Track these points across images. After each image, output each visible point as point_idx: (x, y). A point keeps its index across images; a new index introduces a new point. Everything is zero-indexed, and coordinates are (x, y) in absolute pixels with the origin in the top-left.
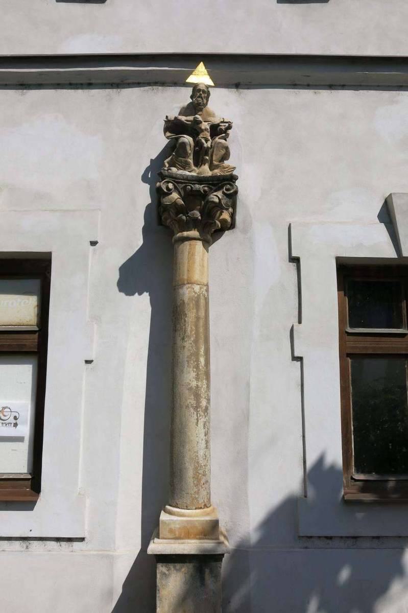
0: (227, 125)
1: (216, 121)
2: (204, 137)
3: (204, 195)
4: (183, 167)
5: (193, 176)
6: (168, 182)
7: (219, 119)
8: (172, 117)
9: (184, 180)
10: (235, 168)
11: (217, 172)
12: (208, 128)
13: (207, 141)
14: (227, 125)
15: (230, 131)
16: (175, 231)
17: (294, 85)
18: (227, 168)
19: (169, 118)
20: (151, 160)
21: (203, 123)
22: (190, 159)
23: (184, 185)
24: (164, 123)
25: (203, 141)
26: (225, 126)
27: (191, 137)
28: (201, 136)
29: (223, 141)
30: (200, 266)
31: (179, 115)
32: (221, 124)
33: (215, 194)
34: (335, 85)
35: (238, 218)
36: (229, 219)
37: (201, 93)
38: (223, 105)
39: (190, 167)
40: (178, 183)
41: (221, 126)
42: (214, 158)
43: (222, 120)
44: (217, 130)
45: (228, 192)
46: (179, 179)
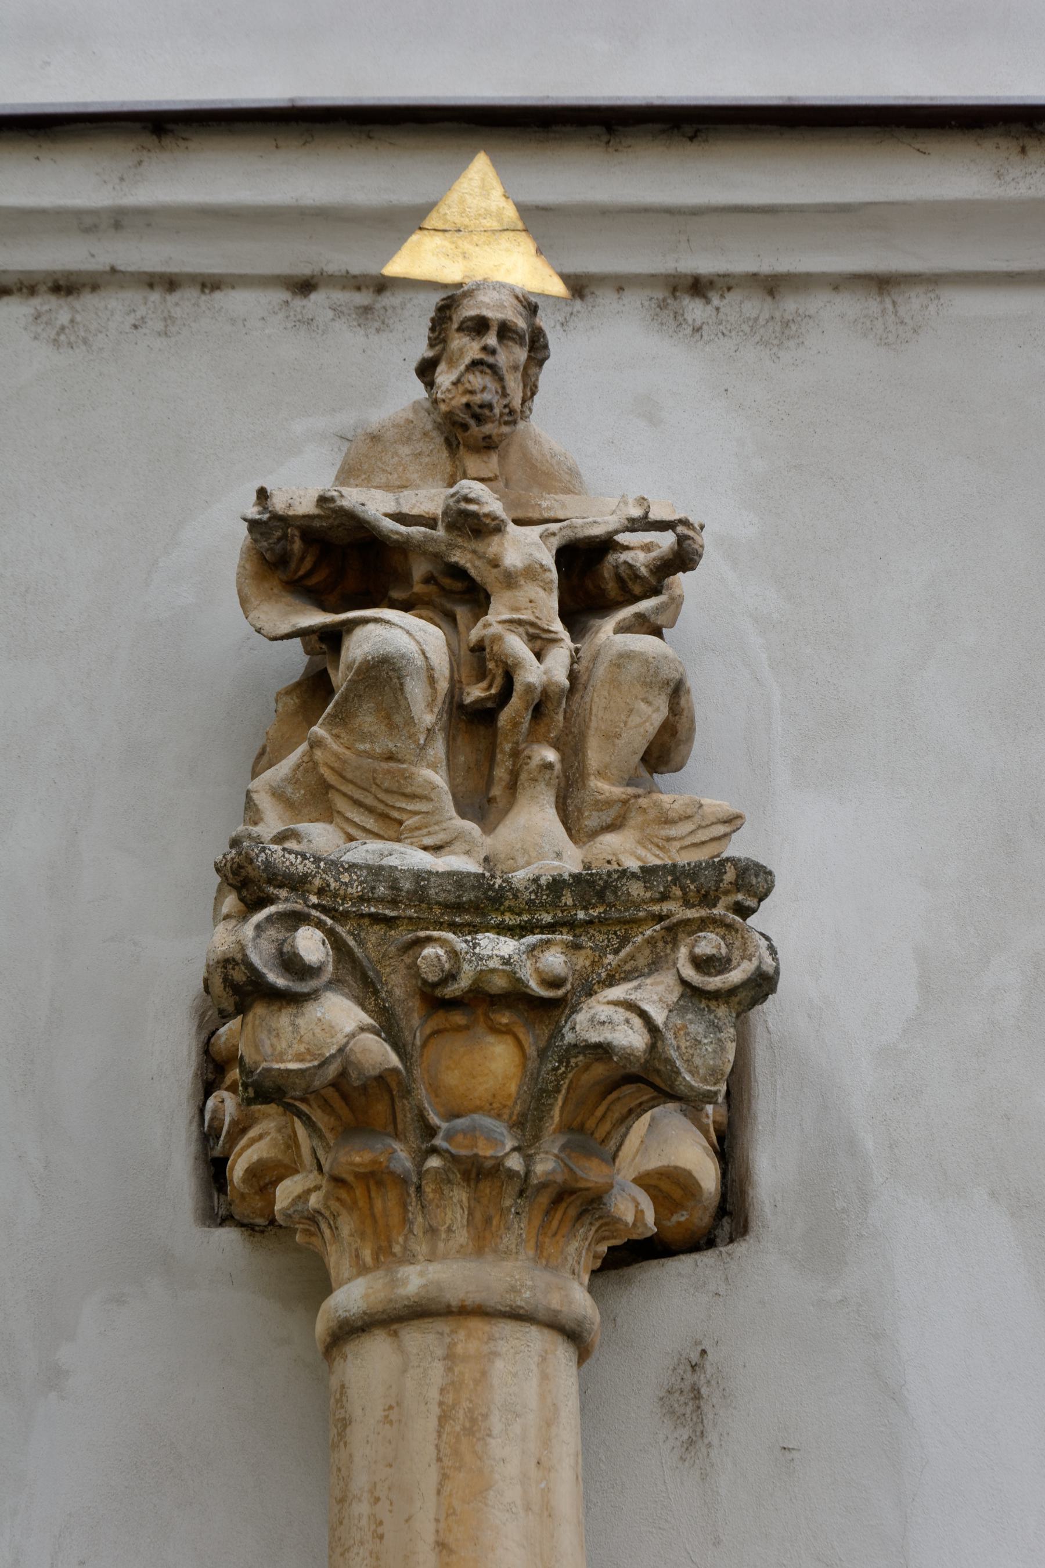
0: (666, 540)
1: (596, 515)
2: (520, 622)
4: (384, 817)
5: (458, 879)
6: (295, 920)
7: (613, 502)
10: (738, 817)
11: (624, 849)
12: (548, 559)
13: (540, 643)
14: (666, 540)
15: (683, 581)
16: (338, 1262)
19: (279, 504)
21: (511, 527)
22: (433, 766)
24: (242, 531)
25: (517, 646)
26: (647, 548)
28: (498, 612)
29: (643, 643)
30: (528, 1508)
31: (348, 473)
32: (623, 538)
33: (618, 992)
35: (772, 1165)
36: (707, 1174)
37: (491, 340)
38: (623, 431)
41: (627, 548)
42: (595, 756)
43: (636, 512)
44: (589, 579)
45: (715, 982)
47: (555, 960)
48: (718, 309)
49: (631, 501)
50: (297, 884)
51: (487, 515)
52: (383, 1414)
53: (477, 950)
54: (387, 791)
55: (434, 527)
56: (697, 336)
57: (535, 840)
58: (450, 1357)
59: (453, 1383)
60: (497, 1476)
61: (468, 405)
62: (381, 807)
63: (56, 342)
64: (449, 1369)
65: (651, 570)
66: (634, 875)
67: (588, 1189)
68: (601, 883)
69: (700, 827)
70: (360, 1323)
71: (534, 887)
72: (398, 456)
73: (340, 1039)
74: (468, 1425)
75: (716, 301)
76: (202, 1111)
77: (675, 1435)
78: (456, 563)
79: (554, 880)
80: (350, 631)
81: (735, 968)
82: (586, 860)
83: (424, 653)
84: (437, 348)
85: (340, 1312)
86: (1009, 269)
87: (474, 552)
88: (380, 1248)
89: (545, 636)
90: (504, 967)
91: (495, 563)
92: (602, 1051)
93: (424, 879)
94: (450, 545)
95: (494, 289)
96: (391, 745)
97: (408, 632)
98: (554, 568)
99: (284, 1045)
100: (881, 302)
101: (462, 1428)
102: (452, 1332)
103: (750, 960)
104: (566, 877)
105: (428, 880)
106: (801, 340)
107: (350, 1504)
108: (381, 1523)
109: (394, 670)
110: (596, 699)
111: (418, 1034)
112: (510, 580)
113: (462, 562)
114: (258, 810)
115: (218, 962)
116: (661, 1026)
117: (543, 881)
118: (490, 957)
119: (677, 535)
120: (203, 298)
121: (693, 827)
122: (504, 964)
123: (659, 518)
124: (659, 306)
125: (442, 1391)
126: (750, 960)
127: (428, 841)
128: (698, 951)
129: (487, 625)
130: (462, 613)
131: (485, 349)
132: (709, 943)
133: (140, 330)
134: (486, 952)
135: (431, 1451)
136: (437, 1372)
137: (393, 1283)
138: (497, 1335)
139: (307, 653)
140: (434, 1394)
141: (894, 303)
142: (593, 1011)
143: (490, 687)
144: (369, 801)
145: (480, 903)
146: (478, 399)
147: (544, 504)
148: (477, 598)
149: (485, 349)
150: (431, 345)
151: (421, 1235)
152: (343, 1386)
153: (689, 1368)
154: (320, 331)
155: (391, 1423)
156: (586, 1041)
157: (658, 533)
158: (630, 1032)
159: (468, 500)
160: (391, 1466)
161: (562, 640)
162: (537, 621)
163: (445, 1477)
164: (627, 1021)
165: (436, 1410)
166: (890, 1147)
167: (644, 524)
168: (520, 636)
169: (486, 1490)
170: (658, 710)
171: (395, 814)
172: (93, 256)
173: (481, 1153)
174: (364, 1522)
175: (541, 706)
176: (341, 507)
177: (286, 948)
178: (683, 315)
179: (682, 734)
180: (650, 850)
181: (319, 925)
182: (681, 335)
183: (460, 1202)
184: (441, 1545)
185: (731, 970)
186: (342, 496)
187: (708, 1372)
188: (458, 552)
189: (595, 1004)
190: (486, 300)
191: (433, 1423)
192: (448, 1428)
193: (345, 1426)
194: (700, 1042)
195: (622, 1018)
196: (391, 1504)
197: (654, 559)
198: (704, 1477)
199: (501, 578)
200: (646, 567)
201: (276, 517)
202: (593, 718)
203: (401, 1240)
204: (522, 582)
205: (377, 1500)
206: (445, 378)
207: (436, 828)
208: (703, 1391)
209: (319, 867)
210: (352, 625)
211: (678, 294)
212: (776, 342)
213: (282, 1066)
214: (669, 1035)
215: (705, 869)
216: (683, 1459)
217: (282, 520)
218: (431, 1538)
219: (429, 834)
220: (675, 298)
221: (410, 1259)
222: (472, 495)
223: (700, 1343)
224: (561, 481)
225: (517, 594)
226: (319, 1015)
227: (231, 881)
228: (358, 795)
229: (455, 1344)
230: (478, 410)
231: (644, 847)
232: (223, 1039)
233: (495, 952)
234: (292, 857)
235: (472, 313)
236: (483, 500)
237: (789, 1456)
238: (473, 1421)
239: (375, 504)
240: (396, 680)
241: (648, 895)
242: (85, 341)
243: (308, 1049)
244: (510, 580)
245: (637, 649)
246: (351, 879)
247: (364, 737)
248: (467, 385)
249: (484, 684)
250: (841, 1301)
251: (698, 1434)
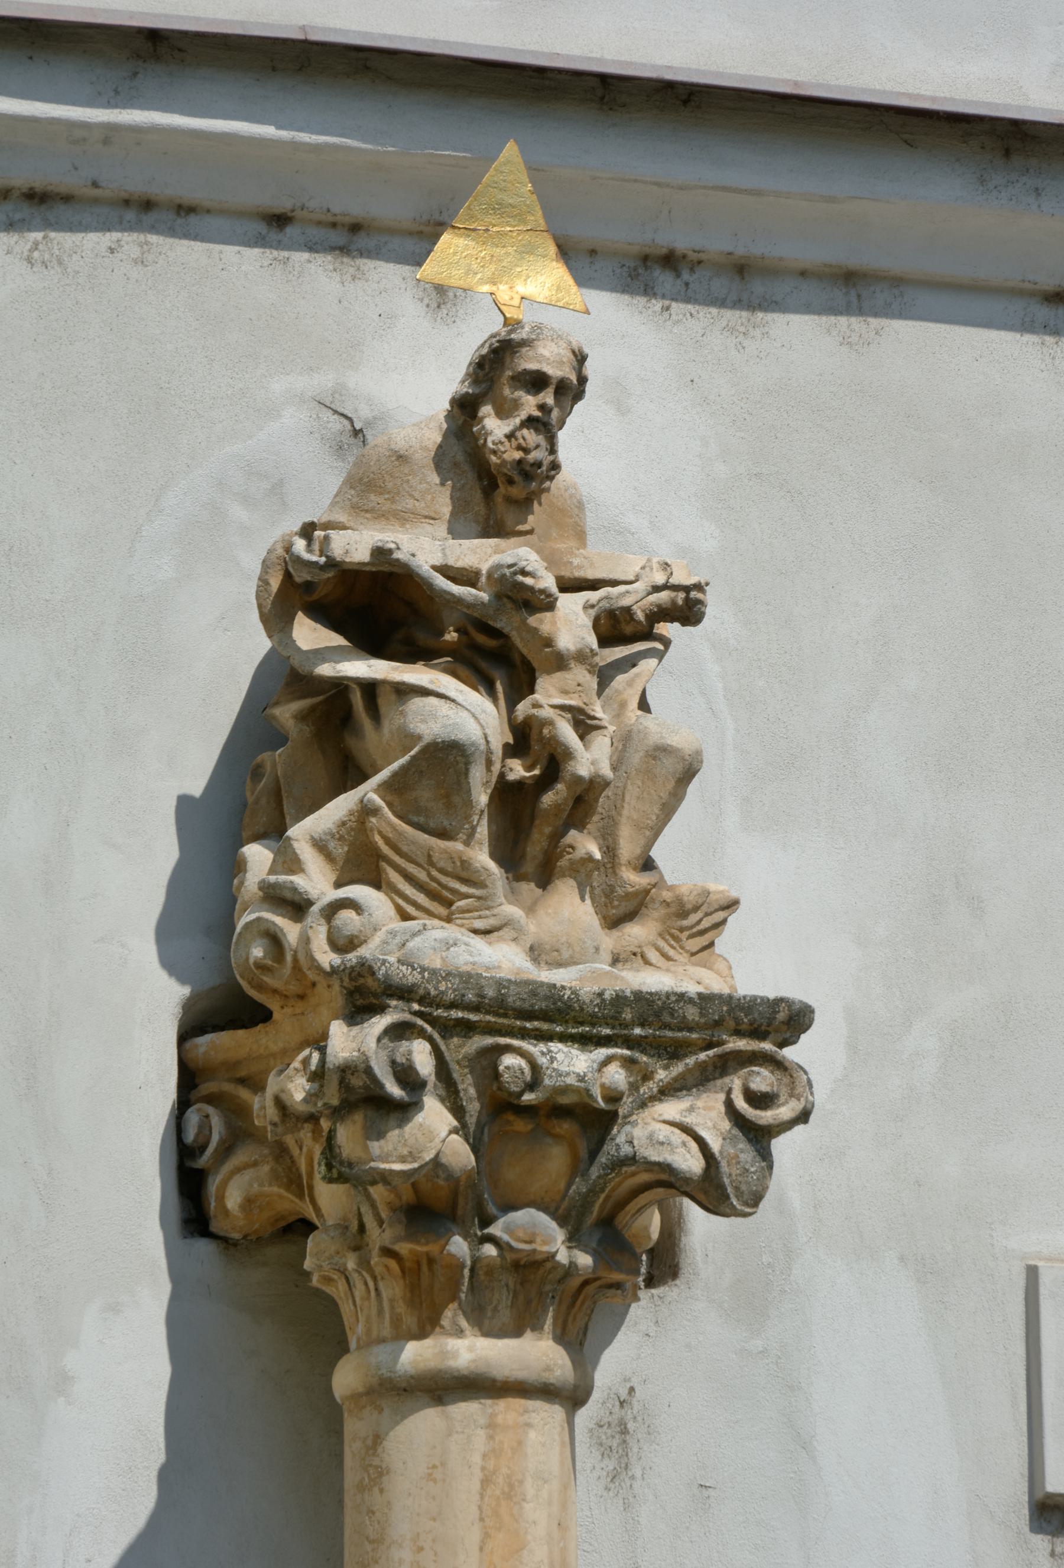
3: (592, 1120)
6: (399, 1032)
9: (476, 1008)
13: (585, 725)
16: (358, 1317)
18: (696, 909)
20: (184, 803)
23: (490, 1040)
25: (566, 732)
33: (672, 1109)
34: (897, 282)
37: (548, 397)
39: (484, 902)
40: (448, 1028)
43: (660, 579)
46: (453, 1005)
47: (617, 1076)
48: (687, 284)
49: (655, 566)
50: (405, 993)
52: (427, 1471)
53: (555, 1065)
54: (442, 871)
56: (666, 314)
58: (491, 1426)
59: (494, 1450)
60: (529, 1537)
61: (520, 462)
63: (29, 260)
64: (491, 1437)
65: (646, 615)
66: (691, 1001)
68: (659, 1003)
69: (707, 914)
70: (404, 1385)
71: (598, 1001)
72: (427, 483)
73: (436, 1144)
74: (506, 1489)
75: (686, 276)
77: (603, 1465)
79: (617, 995)
81: (783, 1105)
82: (615, 951)
83: (486, 738)
84: (484, 386)
85: (384, 1371)
89: (589, 722)
90: (579, 1084)
93: (504, 987)
95: (552, 340)
96: (446, 823)
97: (474, 716)
99: (391, 1147)
100: (847, 294)
101: (501, 1493)
103: (799, 1100)
104: (628, 993)
105: (508, 988)
106: (767, 329)
107: (389, 1547)
109: (462, 755)
111: (486, 1131)
112: (560, 662)
115: (339, 1067)
116: (717, 1154)
117: (607, 996)
118: (568, 1074)
120: (180, 221)
122: (579, 1081)
124: (630, 276)
125: (484, 1456)
126: (799, 1100)
127: (479, 924)
128: (753, 1086)
129: (537, 705)
131: (542, 407)
132: (762, 1080)
133: (116, 255)
134: (564, 1068)
135: (474, 1509)
136: (480, 1437)
138: (531, 1408)
140: (477, 1459)
141: (859, 296)
142: (650, 1128)
144: (422, 876)
145: (555, 1016)
146: (533, 456)
147: (576, 561)
149: (542, 407)
153: (618, 1403)
154: (296, 273)
155: (435, 1481)
156: (645, 1158)
158: (688, 1156)
160: (434, 1520)
161: (606, 728)
162: (584, 706)
163: (486, 1536)
164: (684, 1144)
165: (478, 1474)
166: (815, 1207)
168: (568, 721)
169: (522, 1549)
172: (76, 169)
173: (539, 1248)
176: (398, 560)
177: (400, 1059)
178: (653, 288)
180: (666, 941)
181: (430, 1040)
182: (650, 311)
183: (507, 1285)
185: (779, 1106)
186: (398, 548)
187: (635, 1408)
189: (649, 1120)
190: (546, 353)
191: (476, 1486)
192: (489, 1492)
194: (747, 1170)
195: (679, 1141)
196: (436, 1555)
197: (651, 605)
198: (627, 1506)
200: (643, 611)
202: (626, 805)
204: (572, 665)
205: (421, 1549)
207: (487, 912)
208: (629, 1426)
209: (423, 977)
211: (649, 264)
212: (742, 329)
214: (724, 1164)
215: (760, 1005)
216: (608, 1489)
219: (480, 917)
220: (646, 268)
222: (528, 569)
223: (629, 1380)
224: (571, 517)
225: (567, 676)
226: (420, 1120)
227: (345, 984)
228: (411, 868)
229: (496, 1415)
230: (528, 468)
231: (663, 938)
232: (202, 1050)
233: (572, 1068)
234: (404, 968)
235: (532, 366)
236: (539, 574)
237: (706, 1493)
238: (511, 1486)
240: (461, 765)
241: (703, 1020)
242: (60, 262)
243: (410, 1152)
244: (560, 662)
245: (674, 744)
246: (447, 988)
248: (521, 441)
250: (761, 1352)
251: (623, 1465)
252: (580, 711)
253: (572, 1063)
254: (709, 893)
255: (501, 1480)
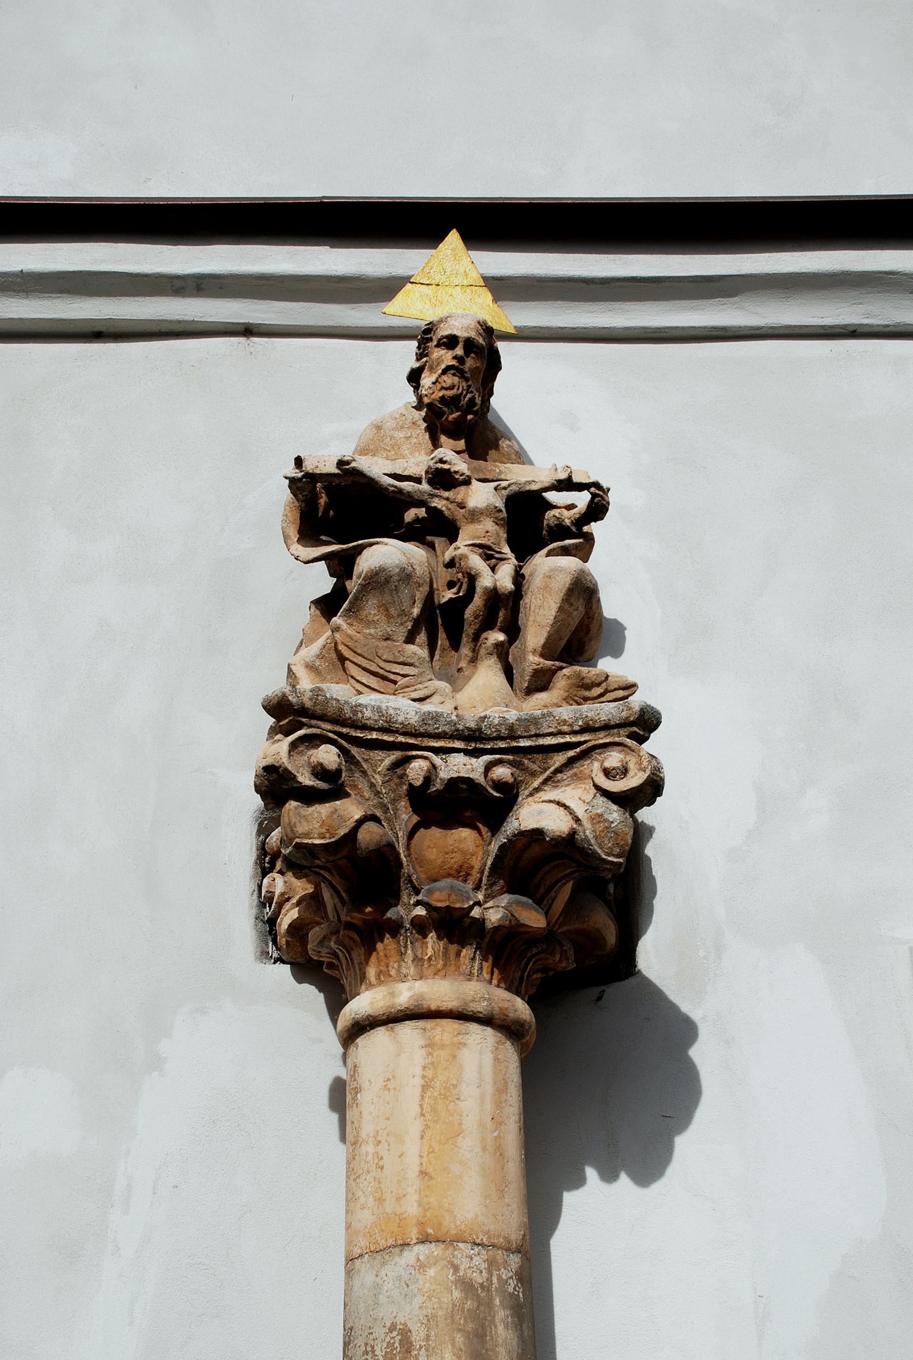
1: (535, 474)
8: (324, 462)
12: (500, 504)
14: (582, 499)
15: (595, 528)
17: (807, 326)
18: (598, 685)
19: (309, 466)
23: (395, 755)
25: (476, 562)
27: (436, 544)
33: (551, 794)
38: (558, 409)
41: (556, 507)
43: (563, 476)
44: (528, 522)
46: (371, 729)
47: (502, 772)
51: (456, 472)
55: (420, 483)
57: (482, 694)
58: (430, 1046)
59: (433, 1063)
62: (381, 672)
67: (529, 932)
76: (260, 887)
78: (435, 507)
80: (360, 553)
86: (823, 324)
87: (447, 499)
88: (381, 971)
89: (497, 555)
91: (462, 506)
92: (538, 833)
94: (431, 495)
96: (389, 629)
98: (504, 510)
102: (432, 1028)
108: (382, 1158)
110: (533, 601)
113: (439, 507)
114: (296, 677)
119: (591, 493)
121: (602, 691)
123: (578, 481)
127: (415, 695)
128: (607, 764)
130: (438, 541)
137: (393, 994)
139: (332, 575)
140: (418, 1071)
143: (458, 592)
144: (373, 668)
148: (450, 531)
150: (418, 360)
151: (410, 962)
152: (355, 1066)
157: (577, 493)
159: (441, 461)
165: (418, 1081)
167: (567, 485)
170: (577, 609)
171: (392, 677)
174: (370, 1157)
175: (494, 596)
179: (594, 630)
184: (423, 1173)
188: (436, 500)
192: (429, 1093)
193: (357, 1093)
199: (467, 515)
201: (308, 475)
203: (396, 965)
206: (427, 380)
210: (359, 550)
213: (310, 841)
217: (312, 478)
218: (417, 1169)
221: (403, 978)
229: (434, 1037)
236: (453, 462)
239: (376, 468)
247: (369, 624)
249: (454, 590)
252: (489, 548)
253: (460, 765)
254: (607, 676)
255: (438, 1085)
